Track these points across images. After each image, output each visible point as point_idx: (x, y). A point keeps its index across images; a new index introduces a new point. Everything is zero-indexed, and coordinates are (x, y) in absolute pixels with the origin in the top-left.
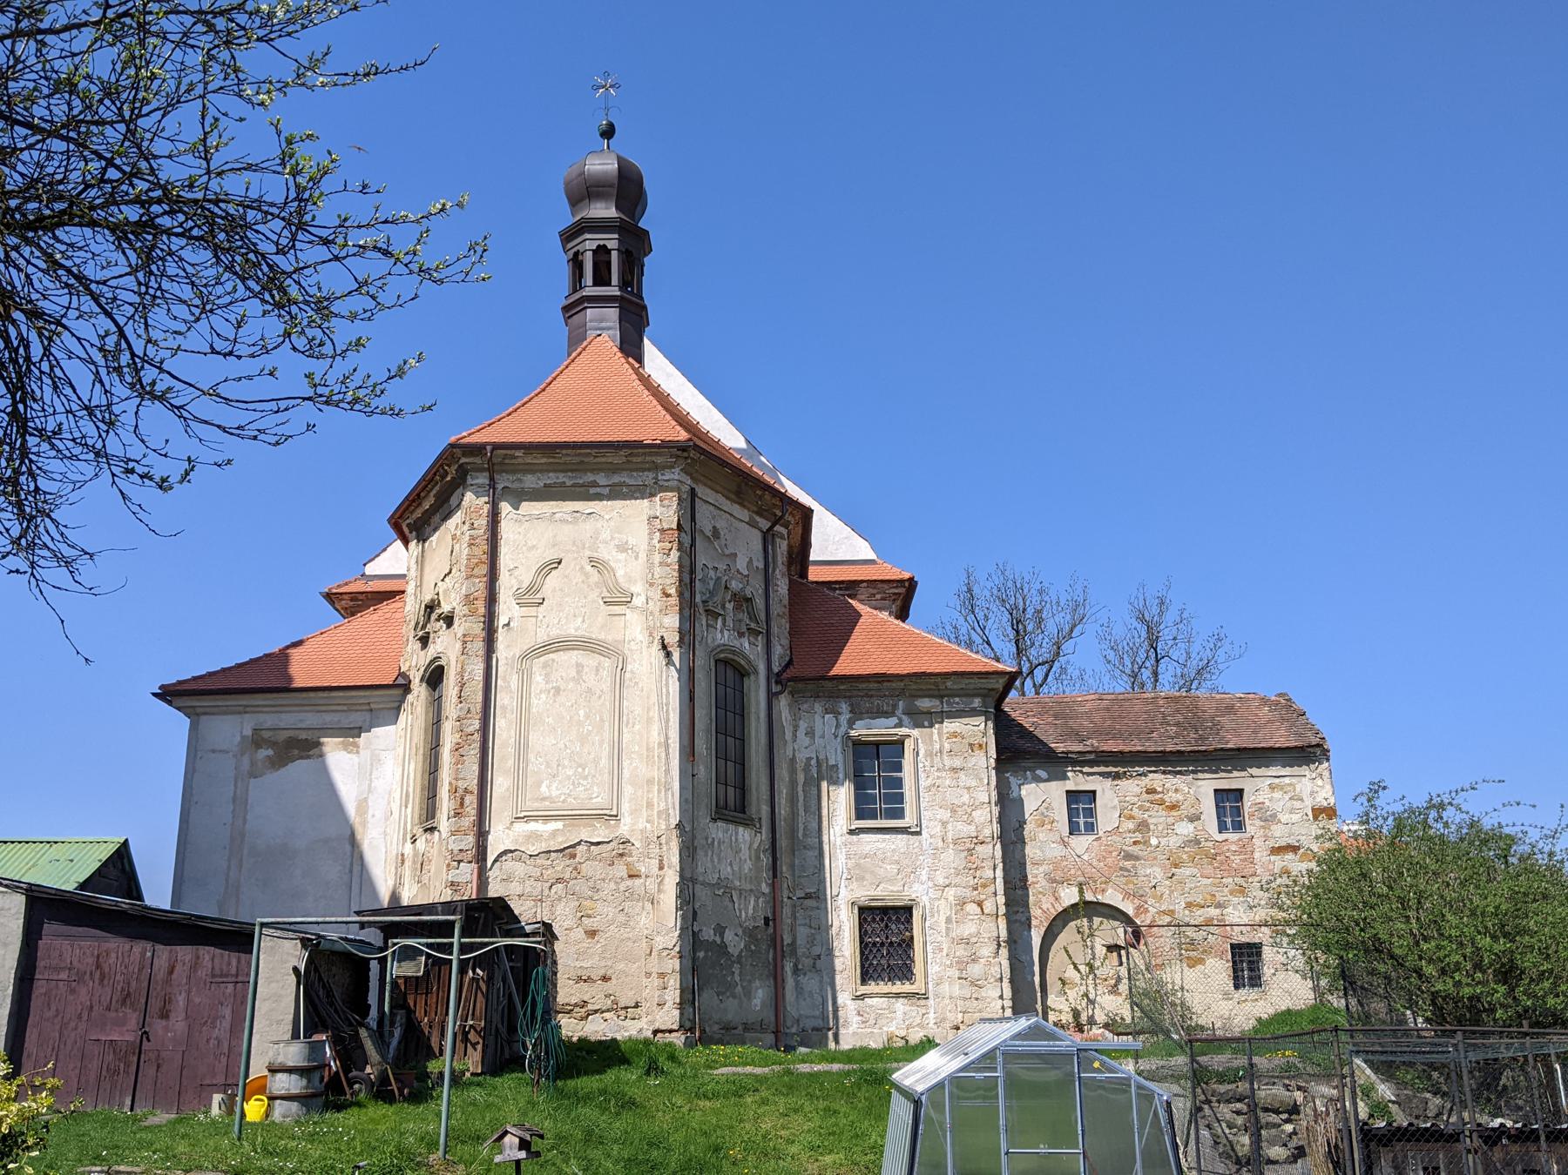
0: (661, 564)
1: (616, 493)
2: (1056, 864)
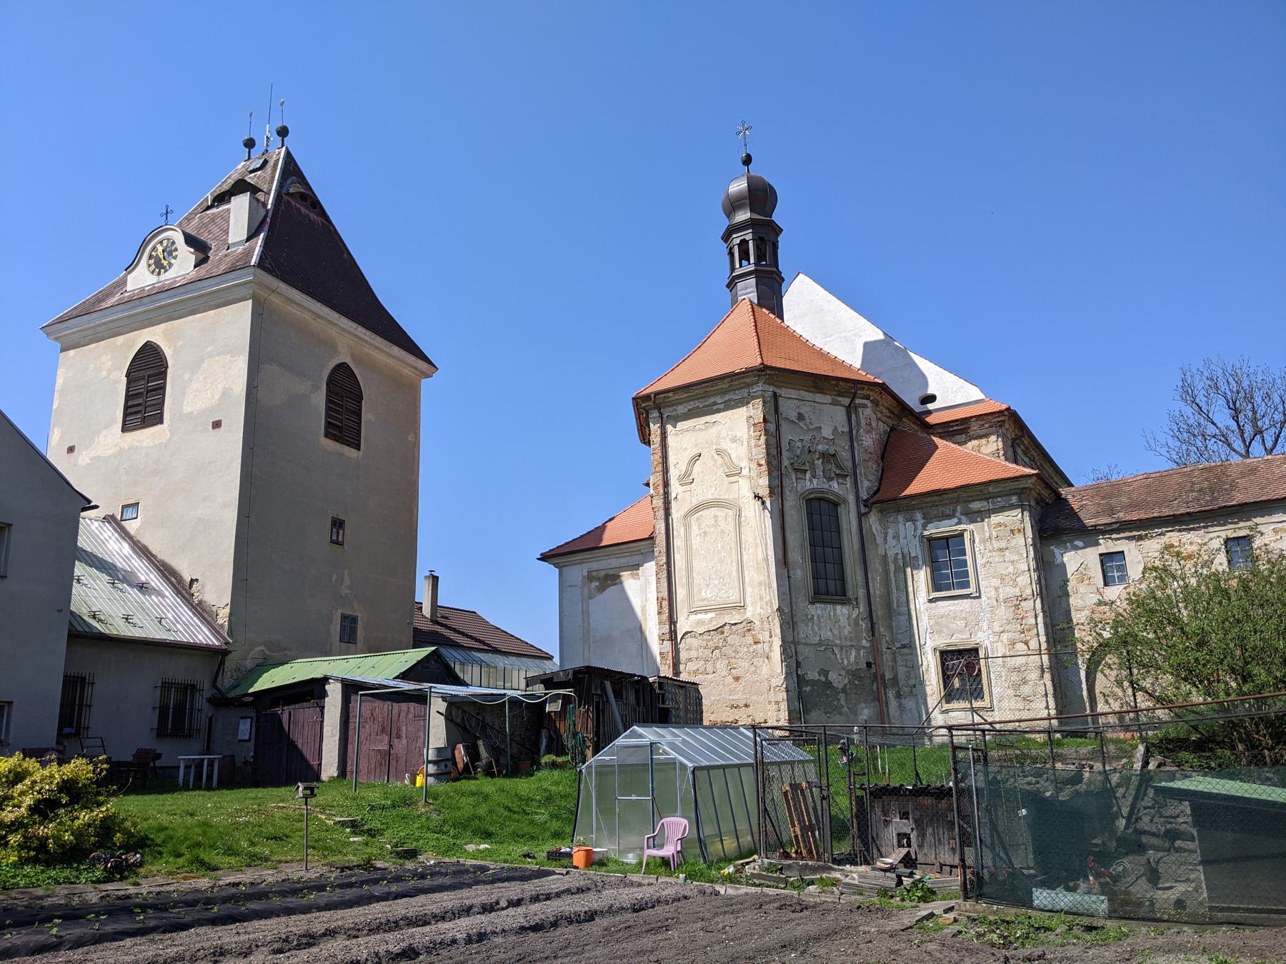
1: (729, 406)
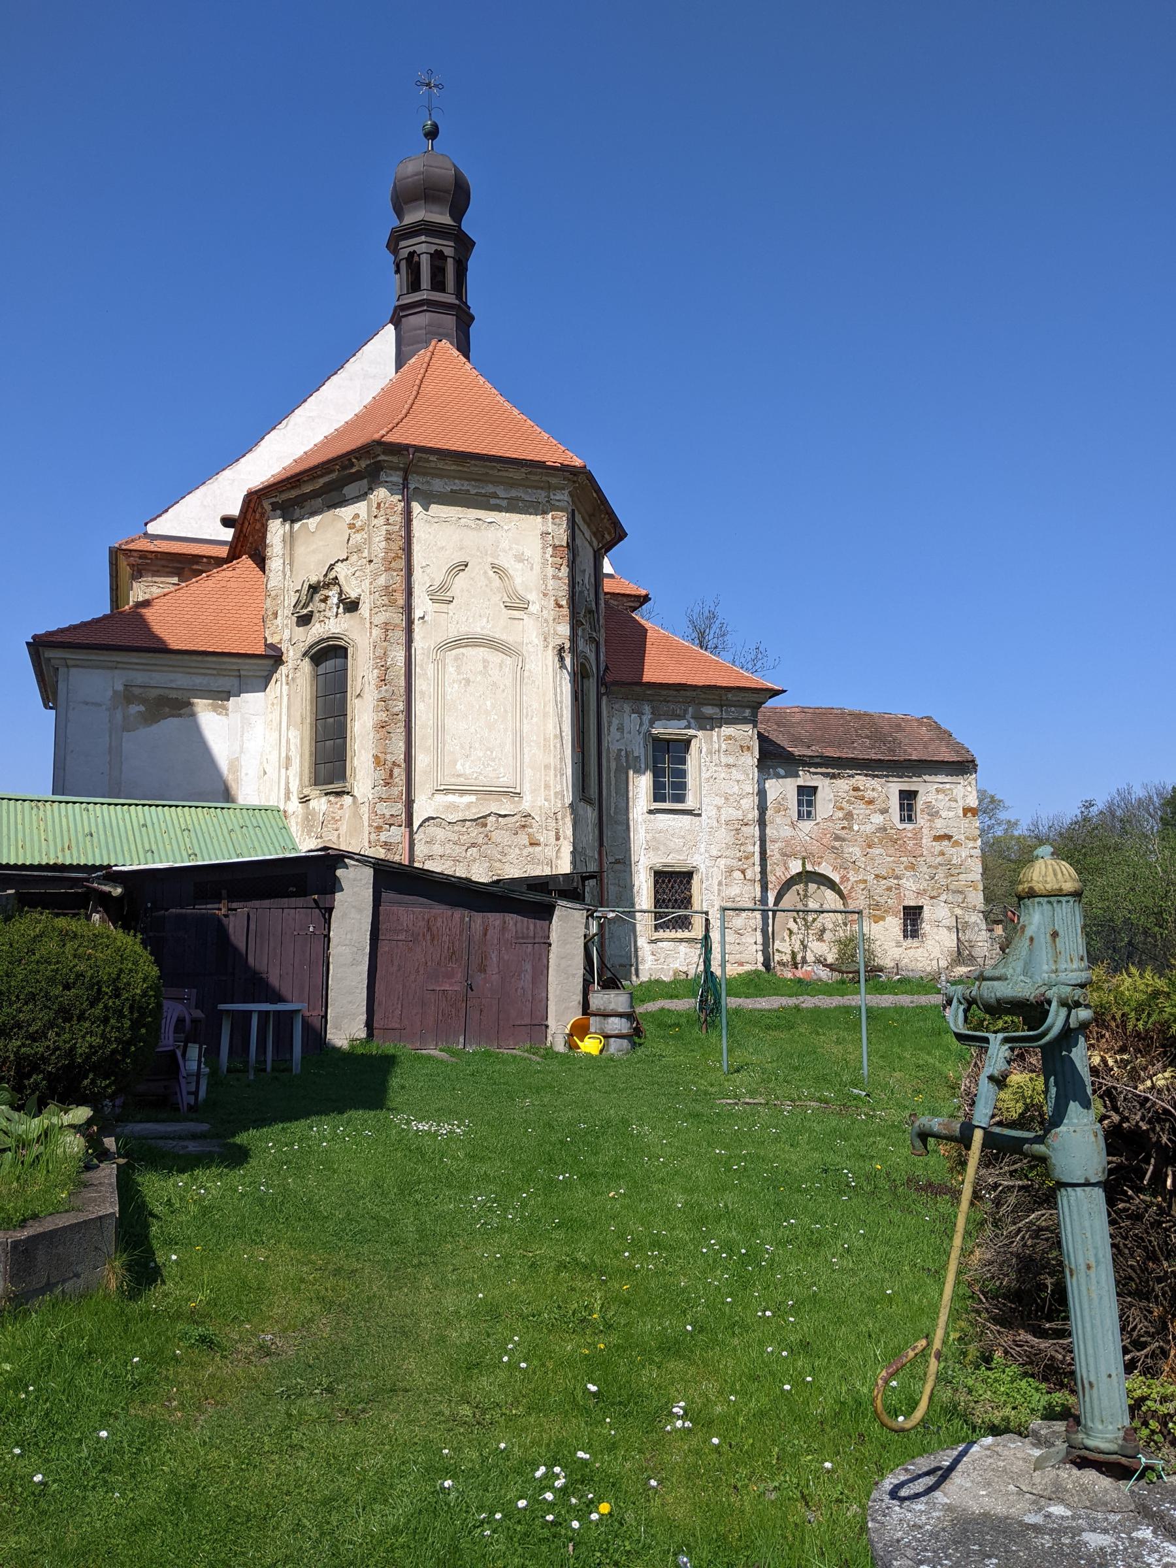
0: (554, 577)
1: (513, 506)
2: (787, 842)
